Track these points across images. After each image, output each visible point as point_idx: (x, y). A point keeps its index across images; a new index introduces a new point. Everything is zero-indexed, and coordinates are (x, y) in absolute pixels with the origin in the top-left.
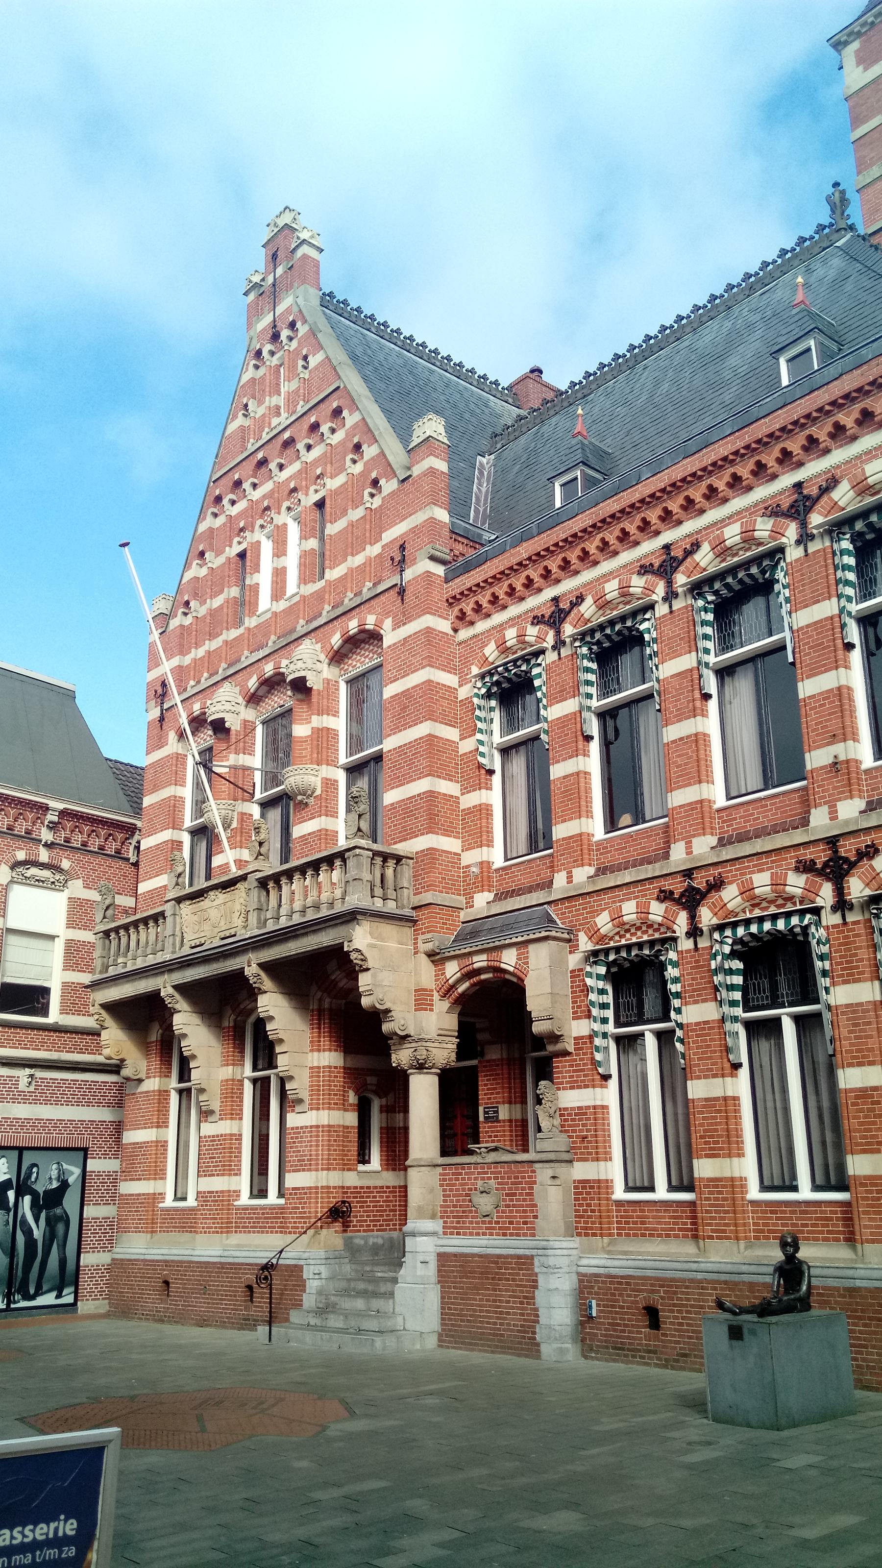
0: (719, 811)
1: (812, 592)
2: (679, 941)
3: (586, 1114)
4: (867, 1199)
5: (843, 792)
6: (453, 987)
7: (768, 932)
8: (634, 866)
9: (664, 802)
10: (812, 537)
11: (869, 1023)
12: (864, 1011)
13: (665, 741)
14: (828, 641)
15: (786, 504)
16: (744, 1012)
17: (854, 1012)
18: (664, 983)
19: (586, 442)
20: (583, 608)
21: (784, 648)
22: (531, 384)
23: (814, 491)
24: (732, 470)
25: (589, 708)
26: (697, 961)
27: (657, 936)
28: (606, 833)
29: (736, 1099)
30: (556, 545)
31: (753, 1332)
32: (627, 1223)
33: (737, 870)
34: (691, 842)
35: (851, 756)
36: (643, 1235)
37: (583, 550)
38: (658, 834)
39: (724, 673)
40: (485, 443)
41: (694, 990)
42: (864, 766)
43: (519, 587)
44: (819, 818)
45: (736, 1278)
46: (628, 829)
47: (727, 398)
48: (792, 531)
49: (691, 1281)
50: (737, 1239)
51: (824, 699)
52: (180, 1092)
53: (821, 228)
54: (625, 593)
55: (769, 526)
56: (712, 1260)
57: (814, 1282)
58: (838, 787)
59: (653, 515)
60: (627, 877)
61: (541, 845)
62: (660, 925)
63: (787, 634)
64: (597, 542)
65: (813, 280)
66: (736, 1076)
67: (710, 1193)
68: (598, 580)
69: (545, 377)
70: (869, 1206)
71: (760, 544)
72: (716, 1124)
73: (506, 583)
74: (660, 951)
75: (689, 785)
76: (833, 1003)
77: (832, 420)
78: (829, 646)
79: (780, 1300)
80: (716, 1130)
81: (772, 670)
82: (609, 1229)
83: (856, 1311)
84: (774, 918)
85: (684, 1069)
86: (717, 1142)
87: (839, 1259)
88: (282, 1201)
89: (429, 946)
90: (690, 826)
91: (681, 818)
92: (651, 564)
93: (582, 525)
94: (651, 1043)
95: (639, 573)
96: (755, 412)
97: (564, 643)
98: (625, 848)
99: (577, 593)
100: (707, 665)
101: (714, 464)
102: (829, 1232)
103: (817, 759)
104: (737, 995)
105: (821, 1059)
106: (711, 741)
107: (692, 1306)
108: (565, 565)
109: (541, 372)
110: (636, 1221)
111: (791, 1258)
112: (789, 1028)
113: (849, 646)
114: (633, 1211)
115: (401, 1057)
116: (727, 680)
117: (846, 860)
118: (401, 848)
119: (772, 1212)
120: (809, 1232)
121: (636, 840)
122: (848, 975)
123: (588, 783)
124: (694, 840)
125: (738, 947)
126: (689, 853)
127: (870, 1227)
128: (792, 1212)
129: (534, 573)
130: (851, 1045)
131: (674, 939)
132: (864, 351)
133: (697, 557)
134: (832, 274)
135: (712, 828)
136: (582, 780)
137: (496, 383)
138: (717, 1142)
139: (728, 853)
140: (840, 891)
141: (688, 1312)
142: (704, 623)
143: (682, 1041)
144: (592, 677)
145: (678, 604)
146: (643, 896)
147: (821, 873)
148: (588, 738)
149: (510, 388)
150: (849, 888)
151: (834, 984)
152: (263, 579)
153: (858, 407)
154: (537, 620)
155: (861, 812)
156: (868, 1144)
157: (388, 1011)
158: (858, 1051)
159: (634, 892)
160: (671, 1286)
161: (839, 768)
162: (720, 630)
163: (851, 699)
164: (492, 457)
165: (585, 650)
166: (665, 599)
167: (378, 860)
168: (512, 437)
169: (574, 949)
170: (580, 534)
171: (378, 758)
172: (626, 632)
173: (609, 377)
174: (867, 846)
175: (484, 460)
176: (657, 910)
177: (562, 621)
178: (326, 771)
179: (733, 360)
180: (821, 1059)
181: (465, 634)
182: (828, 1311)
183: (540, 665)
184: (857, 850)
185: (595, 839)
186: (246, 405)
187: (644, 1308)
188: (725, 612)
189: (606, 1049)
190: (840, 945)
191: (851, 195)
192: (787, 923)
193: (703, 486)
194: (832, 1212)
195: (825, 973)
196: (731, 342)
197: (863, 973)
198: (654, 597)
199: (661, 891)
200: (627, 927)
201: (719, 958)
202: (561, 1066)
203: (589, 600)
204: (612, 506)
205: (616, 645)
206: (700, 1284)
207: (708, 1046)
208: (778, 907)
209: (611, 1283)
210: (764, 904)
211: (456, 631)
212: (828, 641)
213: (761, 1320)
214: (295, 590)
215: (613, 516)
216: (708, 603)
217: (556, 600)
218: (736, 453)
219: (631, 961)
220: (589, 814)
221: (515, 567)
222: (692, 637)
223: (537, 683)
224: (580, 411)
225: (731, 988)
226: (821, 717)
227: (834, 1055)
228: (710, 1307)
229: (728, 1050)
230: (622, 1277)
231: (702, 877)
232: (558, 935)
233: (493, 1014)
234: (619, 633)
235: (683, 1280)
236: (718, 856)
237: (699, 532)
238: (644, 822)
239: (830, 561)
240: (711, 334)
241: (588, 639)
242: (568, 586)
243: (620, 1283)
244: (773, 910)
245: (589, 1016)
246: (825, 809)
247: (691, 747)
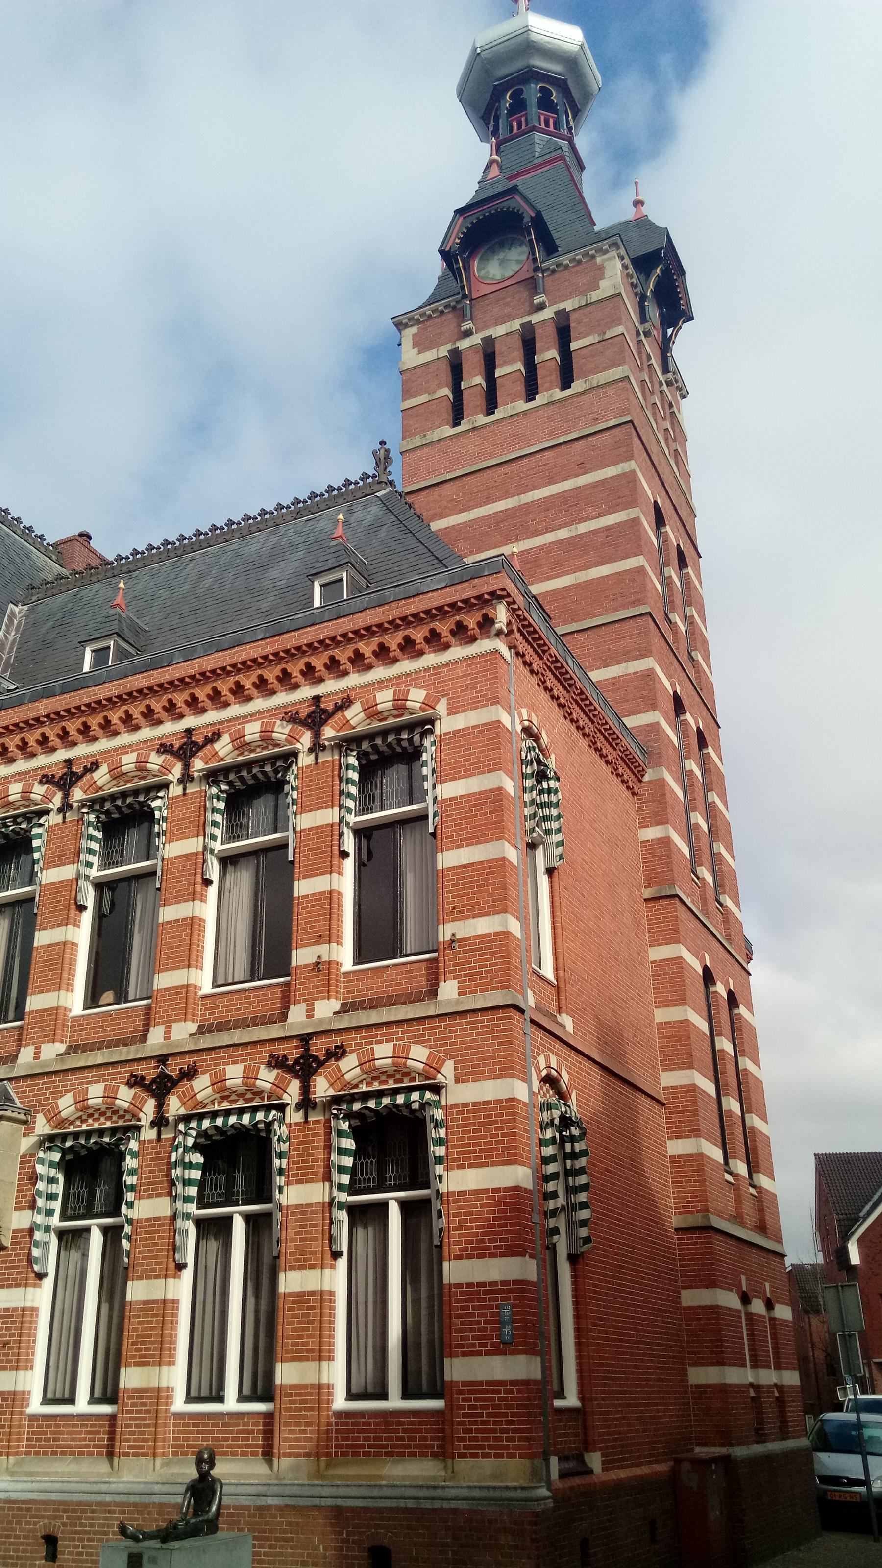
0: (204, 997)
1: (319, 798)
2: (143, 1130)
3: (12, 1316)
4: (288, 1410)
5: (321, 992)
7: (232, 1126)
8: (108, 1047)
9: (150, 981)
10: (324, 748)
11: (316, 1225)
12: (312, 1212)
13: (161, 921)
14: (326, 846)
15: (304, 713)
16: (198, 1208)
17: (303, 1213)
18: (121, 1173)
19: (123, 615)
20: (96, 775)
21: (286, 846)
22: (77, 546)
24: (259, 672)
25: (87, 877)
26: (158, 1153)
27: (121, 1123)
28: (85, 1009)
29: (175, 1302)
30: (78, 708)
31: (153, 1560)
32: (37, 1440)
33: (211, 1059)
34: (170, 1027)
35: (334, 958)
36: (54, 1453)
37: (106, 718)
38: (139, 1016)
39: (228, 861)
40: (20, 593)
41: (150, 1184)
42: (344, 969)
43: (32, 743)
44: (297, 1014)
45: (146, 1499)
46: (109, 1007)
47: (265, 606)
48: (306, 739)
49: (99, 1504)
50: (154, 1455)
51: (316, 900)
53: (365, 477)
54: (141, 767)
55: (287, 730)
56: (125, 1479)
57: (226, 1501)
58: (318, 987)
59: (180, 699)
60: (99, 1058)
61: (11, 1015)
62: (126, 1111)
63: (290, 834)
64: (120, 713)
65: (352, 520)
66: (179, 1277)
67: (133, 1405)
68: (116, 750)
69: (93, 543)
70: (291, 1417)
71: (276, 745)
72: (151, 1329)
73: (20, 736)
74: (122, 1139)
75: (177, 968)
76: (284, 1203)
77: (352, 647)
78: (326, 852)
79: (187, 1523)
80: (150, 1336)
81: (273, 869)
82: (18, 1447)
83: (264, 1531)
84: (241, 1112)
85: (127, 1268)
86: (149, 1349)
87: (254, 1475)
90: (173, 1010)
91: (165, 1001)
92: (172, 745)
93: (107, 694)
94: (96, 1240)
95: (158, 751)
96: (287, 624)
97: (71, 807)
98: (102, 1026)
99: (93, 759)
100: (212, 851)
101: (244, 663)
102: (248, 1446)
103: (302, 956)
104: (193, 1191)
105: (266, 1261)
106: (205, 922)
107: (95, 1533)
108: (85, 730)
109: (90, 538)
110: (49, 1438)
111: (204, 1476)
112: (239, 1228)
113: (344, 854)
114: (48, 1426)
116: (230, 868)
117: (315, 1058)
119: (194, 1425)
120: (229, 1446)
121: (115, 1019)
122: (303, 1175)
123: (74, 954)
124: (175, 1026)
125: (201, 1140)
126: (168, 1038)
127: (289, 1440)
128: (214, 1425)
129: (51, 732)
130: (296, 1247)
131: (138, 1128)
132: (387, 593)
133: (217, 746)
134: (369, 519)
135: (193, 1015)
136: (68, 951)
137: (42, 537)
138: (149, 1349)
139: (205, 1042)
140: (306, 1090)
141: (89, 1540)
142: (214, 810)
143: (129, 1238)
144: (95, 846)
145: (192, 789)
146: (113, 1080)
147: (290, 1070)
148: (82, 908)
149: (56, 545)
150: (315, 1086)
151: (288, 1183)
153: (376, 640)
154: (46, 779)
155: (335, 1013)
156: (297, 1351)
158: (301, 1254)
159: (104, 1075)
160: (74, 1511)
161: (322, 969)
162: (229, 820)
163: (340, 904)
164: (26, 608)
165: (92, 818)
166: (181, 781)
168: (49, 593)
170: (104, 702)
172: (137, 806)
173: (156, 559)
174: (336, 1047)
175: (17, 610)
176: (125, 1096)
177: (73, 784)
179: (274, 573)
180: (266, 1261)
182: (236, 1533)
183: (41, 825)
184: (327, 1049)
185: (72, 1014)
187: (43, 1537)
188: (237, 804)
189: (47, 1244)
190: (300, 1143)
191: (394, 454)
192: (252, 1118)
194: (254, 1424)
195: (281, 1172)
196: (276, 555)
197: (316, 1173)
198: (170, 777)
199: (132, 1076)
200: (91, 1111)
201: (181, 1150)
203: (104, 769)
204: (141, 681)
205: (126, 818)
206: (105, 1506)
207: (156, 1244)
208: (247, 1100)
209: (9, 1509)
210: (234, 1097)
212: (326, 846)
213: (164, 1546)
215: (140, 691)
216: (222, 791)
217: (69, 762)
218: (265, 657)
219: (89, 1149)
220: (70, 988)
221: (31, 722)
222: (202, 822)
223: (36, 843)
224: (122, 585)
225: (187, 1183)
226: (311, 917)
227: (278, 1257)
228: (114, 1533)
229: (175, 1249)
230: (23, 1502)
231: (176, 1064)
232: (14, 1115)
234: (130, 806)
235: (89, 1504)
236: (196, 1044)
237: (221, 723)
238: (127, 1001)
239: (336, 773)
240: (258, 544)
241: (97, 807)
242: (82, 750)
243: (20, 1509)
244: (241, 1104)
245: (33, 1206)
246: (303, 1007)
247: (184, 930)
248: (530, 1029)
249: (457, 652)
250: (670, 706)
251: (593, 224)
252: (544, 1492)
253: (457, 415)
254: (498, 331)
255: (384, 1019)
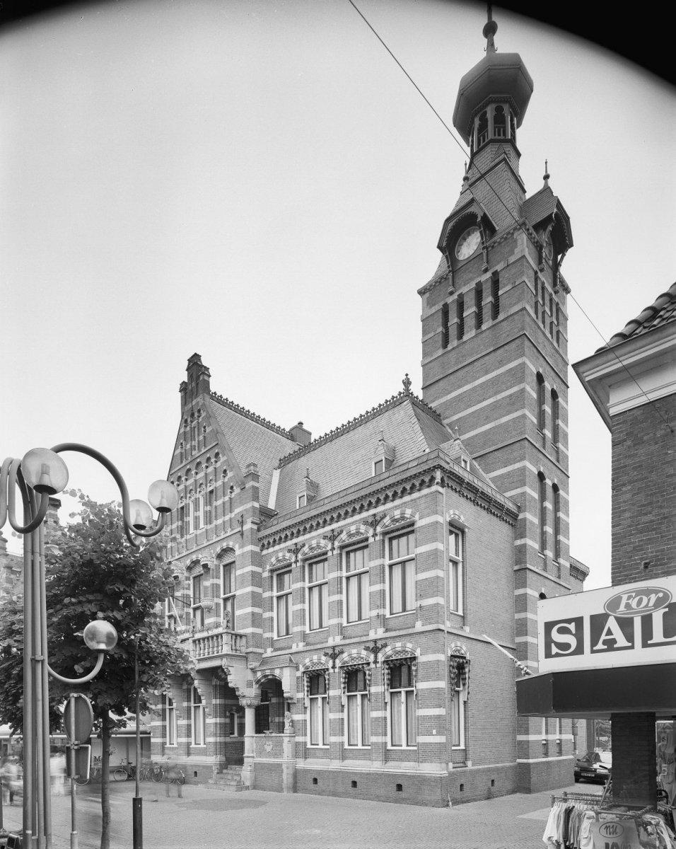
6: (260, 680)
15: (370, 521)
23: (379, 519)
52: (170, 709)
53: (400, 393)
69: (305, 427)
88: (205, 746)
89: (251, 667)
97: (298, 561)
109: (302, 424)
115: (243, 702)
118: (241, 632)
133: (342, 536)
152: (191, 519)
154: (290, 551)
157: (237, 688)
167: (234, 637)
169: (298, 670)
171: (234, 596)
178: (216, 600)
181: (265, 552)
186: (182, 443)
193: (376, 497)
202: (293, 709)
211: (262, 551)
214: (203, 526)
217: (374, 515)
233: (271, 688)
237: (342, 526)
248: (446, 635)
249: (425, 491)
250: (537, 479)
251: (524, 191)
252: (446, 772)
253: (446, 342)
254: (464, 290)
255: (404, 633)
